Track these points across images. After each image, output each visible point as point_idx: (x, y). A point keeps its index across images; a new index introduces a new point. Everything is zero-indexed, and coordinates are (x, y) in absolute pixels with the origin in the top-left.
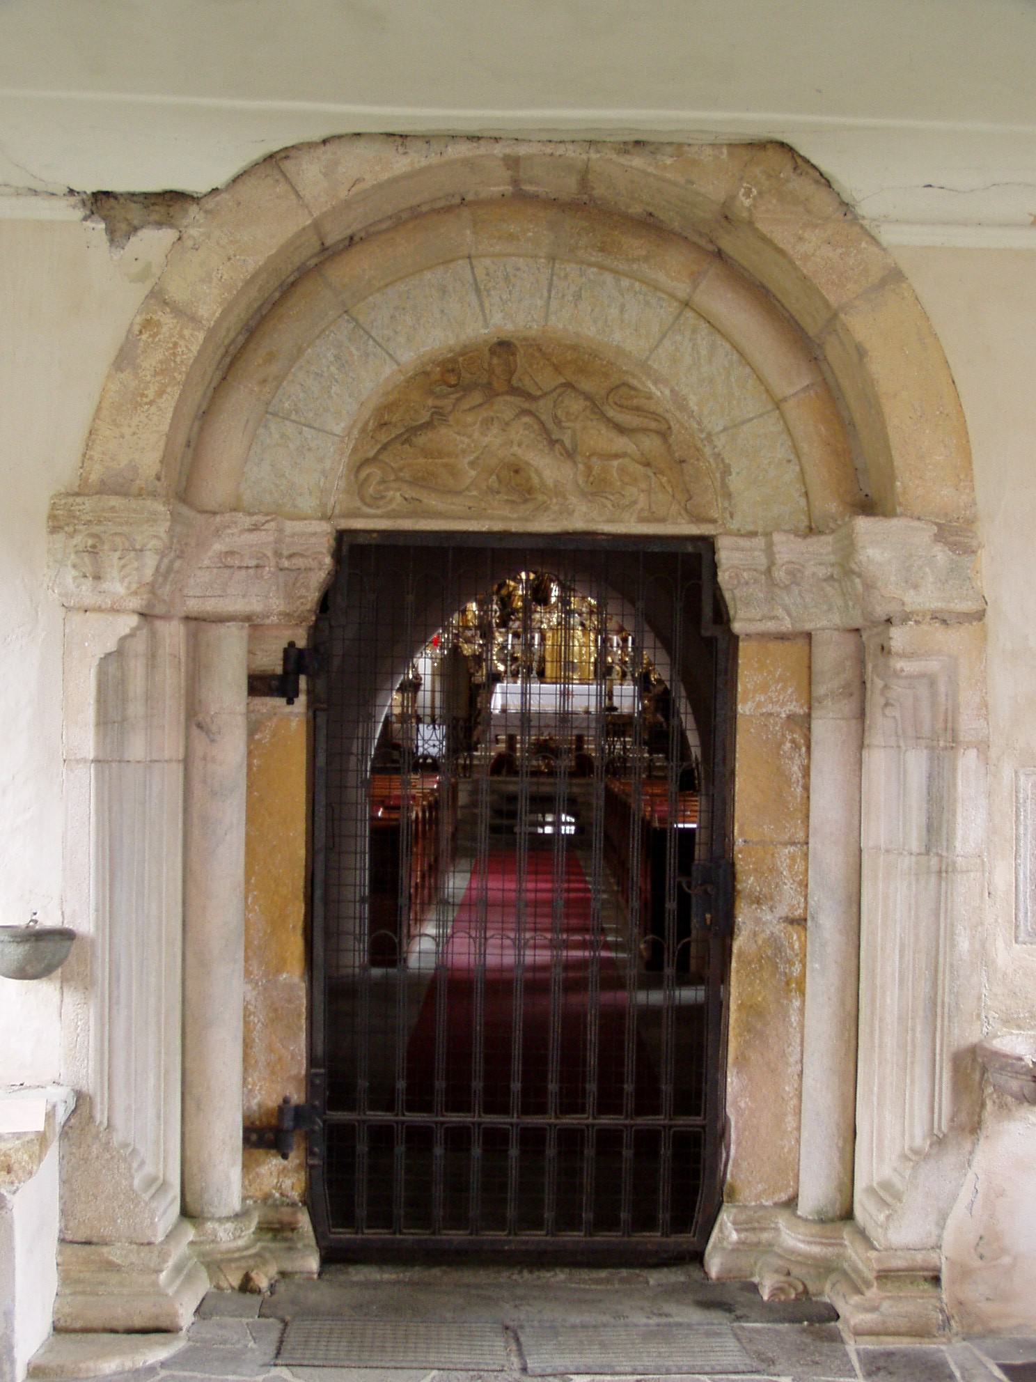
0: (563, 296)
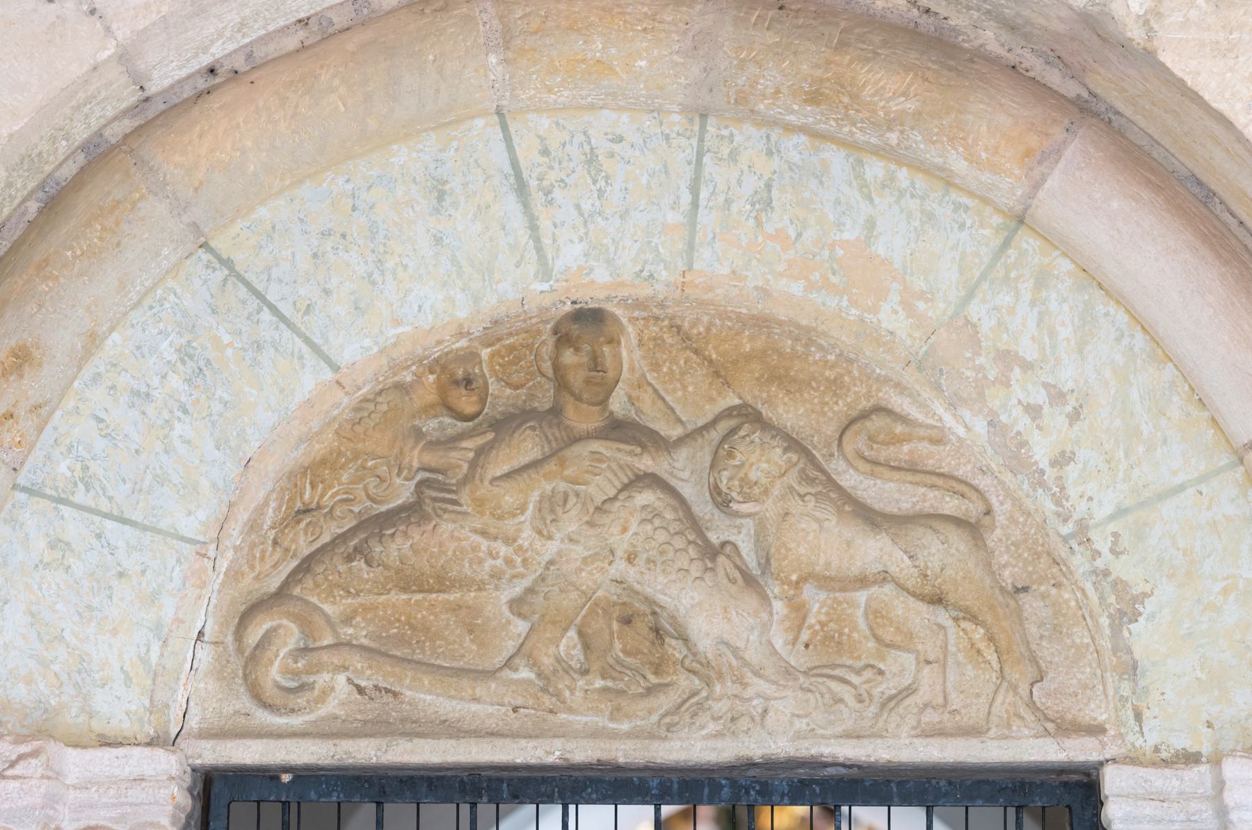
0: (728, 202)
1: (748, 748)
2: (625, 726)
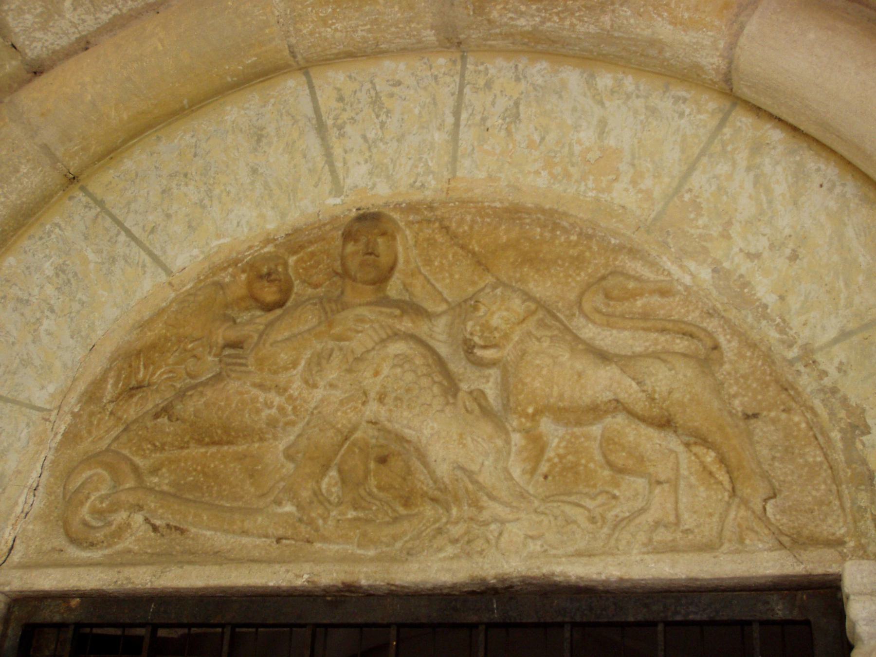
0: (484, 120)
1: (482, 568)
2: (371, 553)
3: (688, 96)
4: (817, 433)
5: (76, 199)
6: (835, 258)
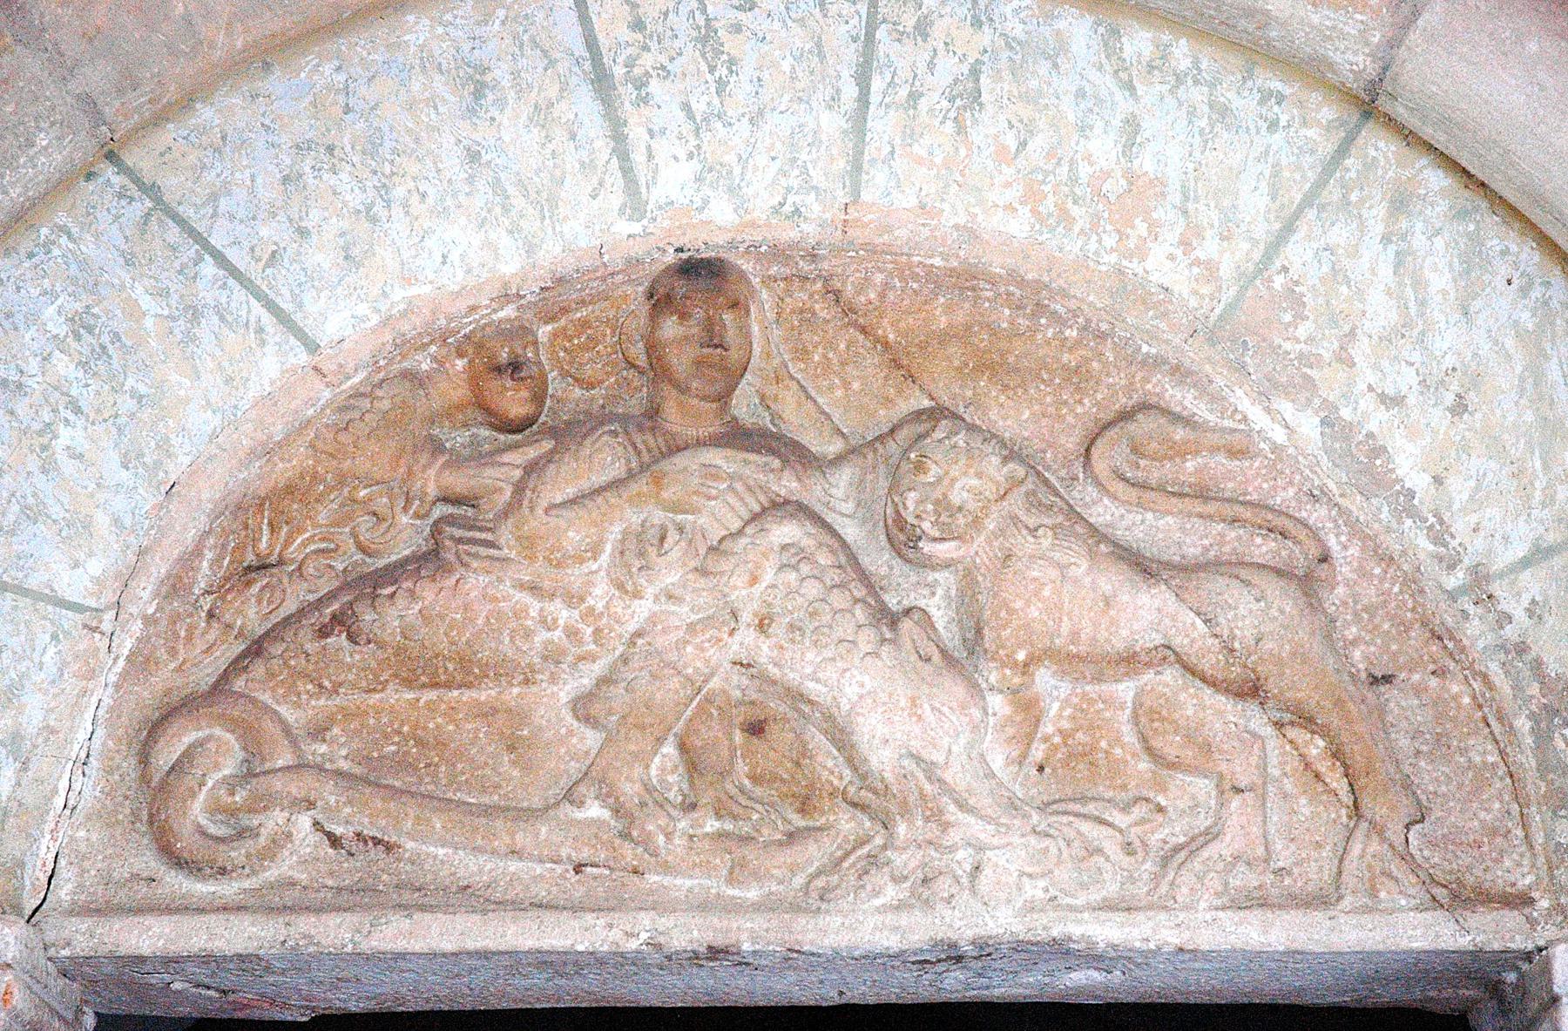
0: (914, 97)
3: (1287, 91)
4: (1490, 716)
5: (101, 180)
6: (1529, 416)
